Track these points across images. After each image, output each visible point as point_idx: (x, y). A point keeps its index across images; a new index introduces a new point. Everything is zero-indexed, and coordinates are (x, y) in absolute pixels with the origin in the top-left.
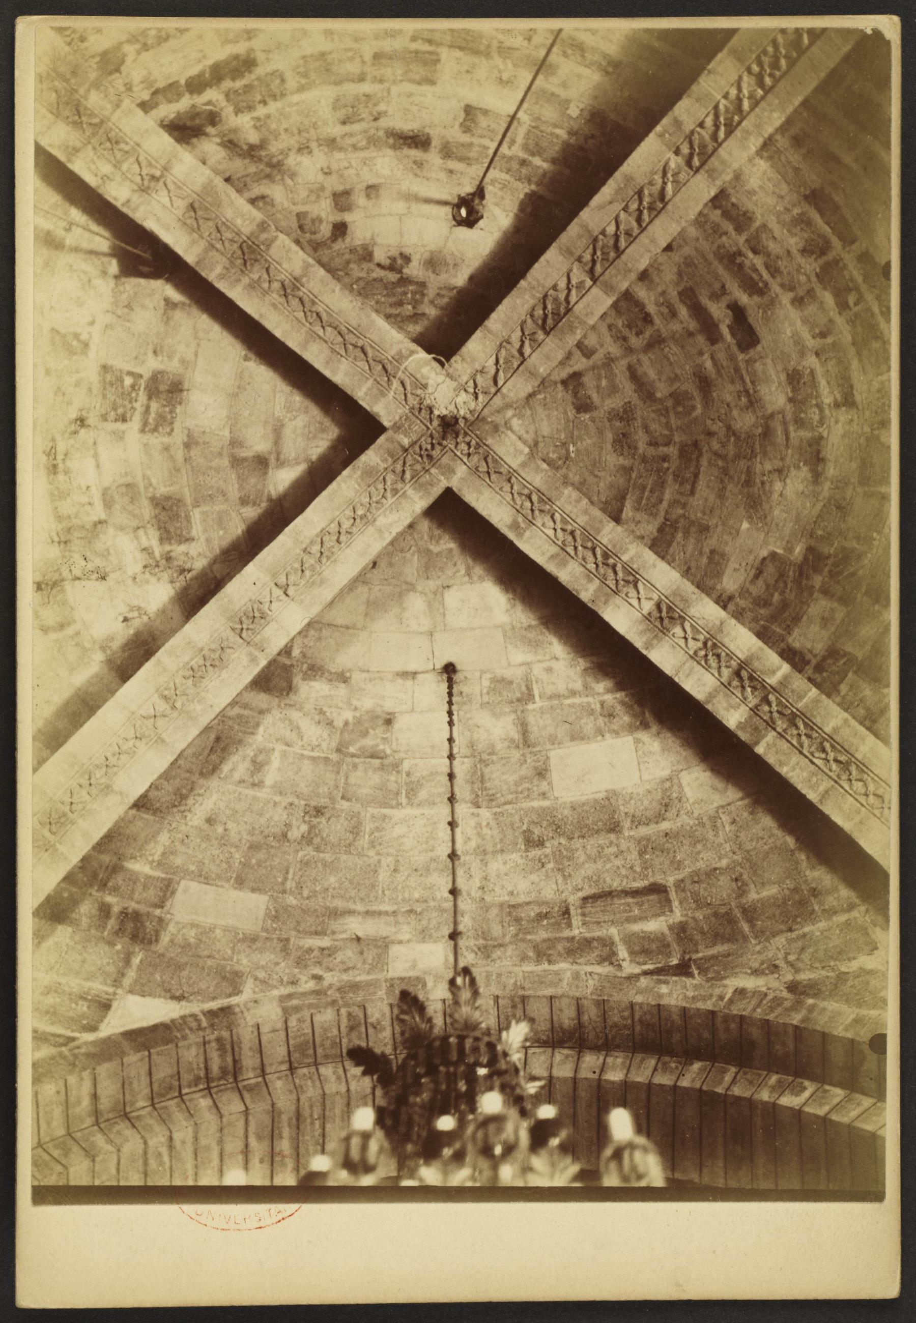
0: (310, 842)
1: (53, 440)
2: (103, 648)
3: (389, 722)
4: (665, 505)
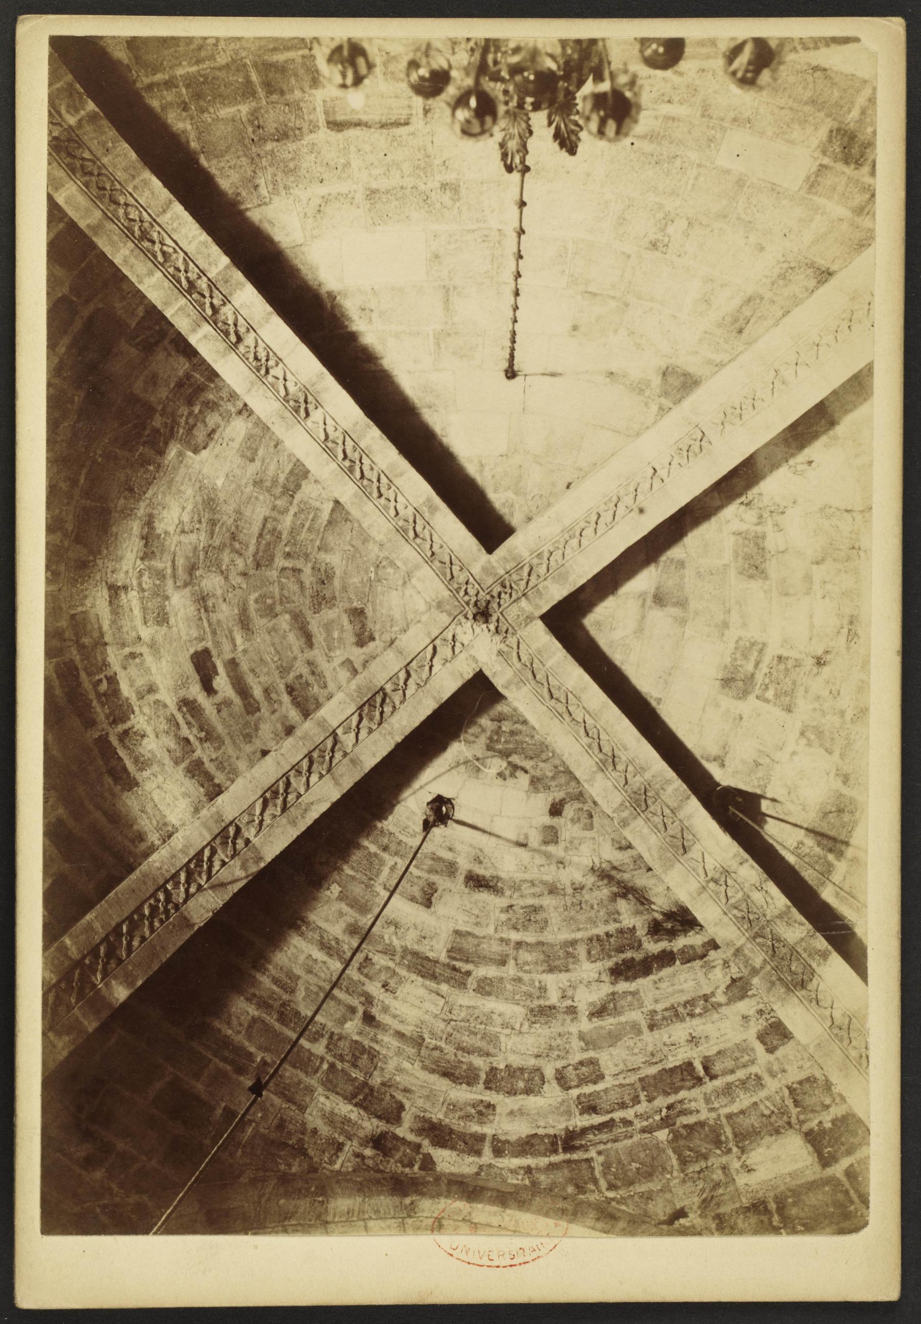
0: (667, 214)
1: (848, 648)
2: (836, 438)
3: (575, 328)
4: (292, 512)
